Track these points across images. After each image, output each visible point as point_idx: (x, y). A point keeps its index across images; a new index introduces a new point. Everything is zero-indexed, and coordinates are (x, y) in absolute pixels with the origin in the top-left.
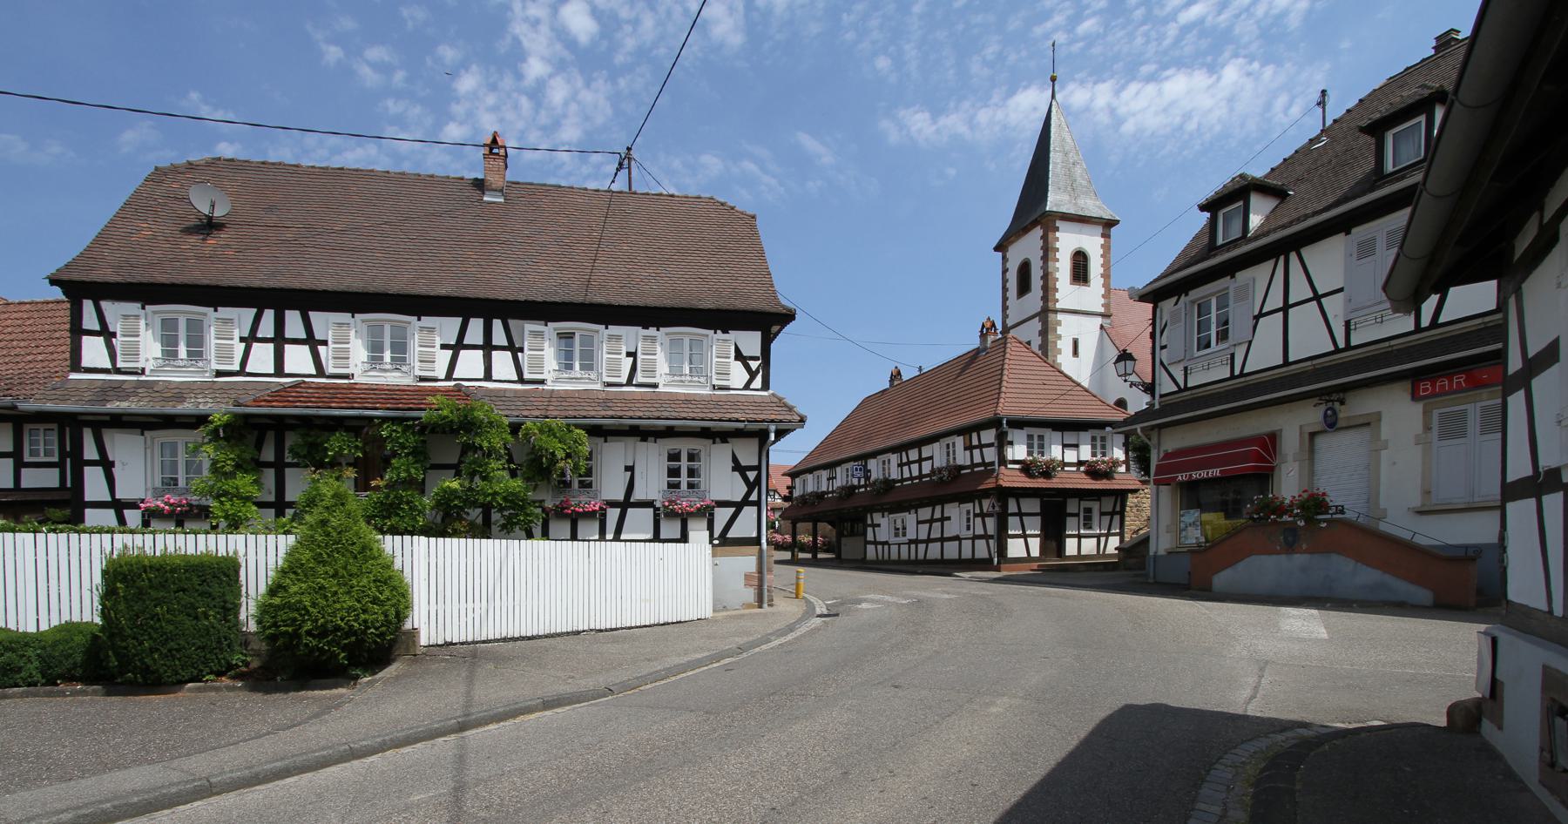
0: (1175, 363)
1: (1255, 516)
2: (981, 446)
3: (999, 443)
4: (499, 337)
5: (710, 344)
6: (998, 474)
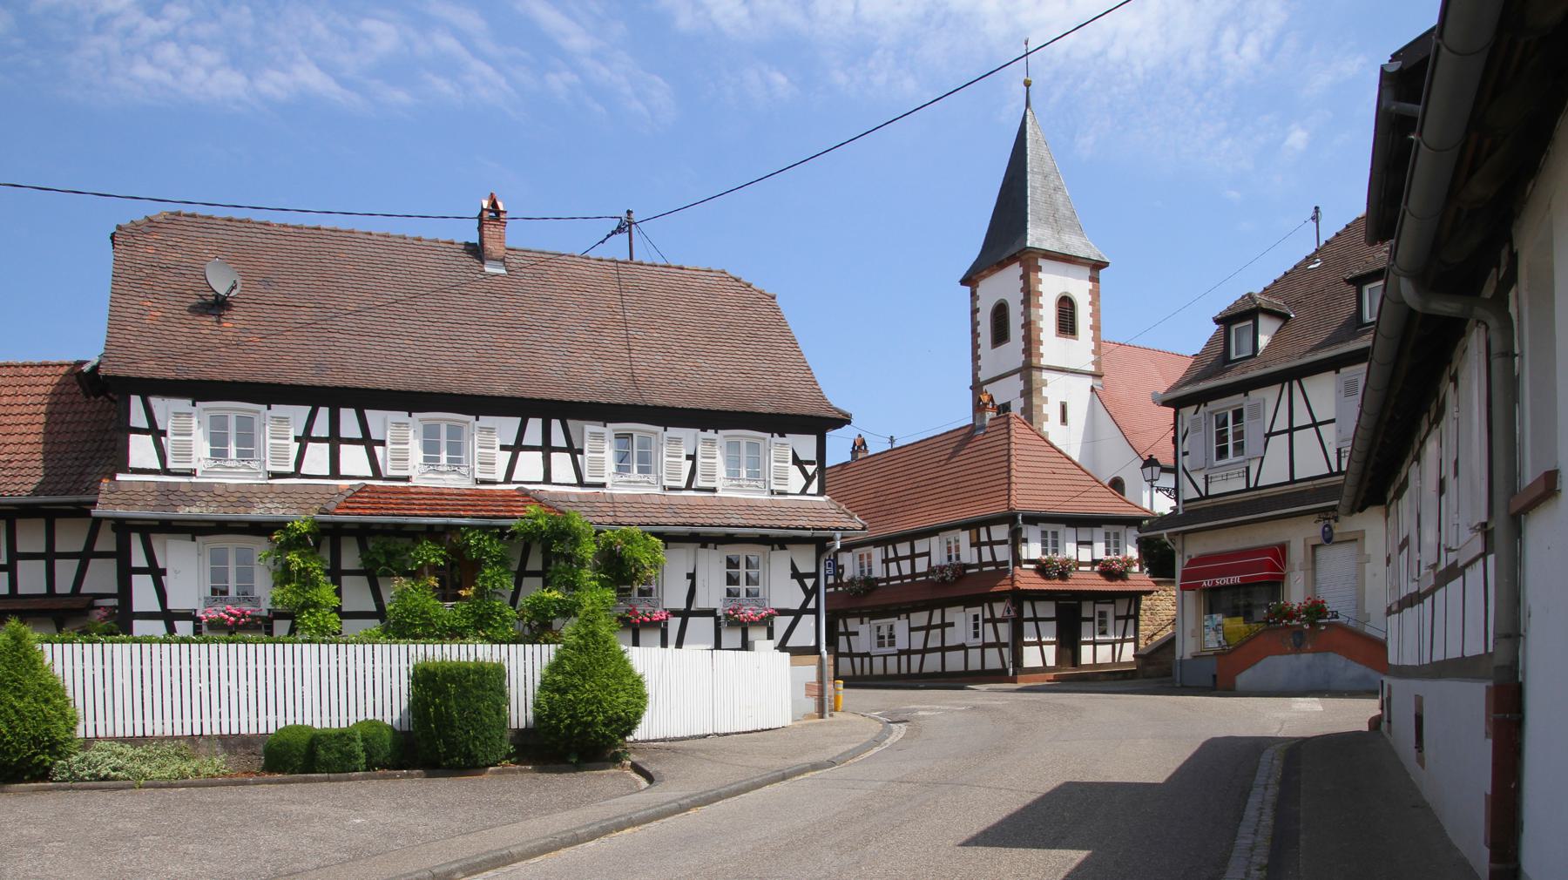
2: (991, 543)
3: (1013, 541)
4: (558, 439)
6: (1013, 576)
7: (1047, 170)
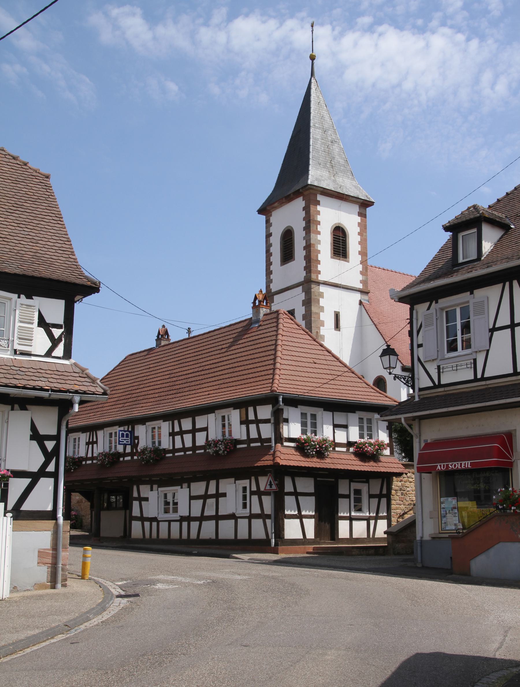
0: (430, 361)
1: (500, 507)
2: (257, 422)
3: (275, 420)
5: (13, 307)
6: (274, 452)
7: (326, 126)
